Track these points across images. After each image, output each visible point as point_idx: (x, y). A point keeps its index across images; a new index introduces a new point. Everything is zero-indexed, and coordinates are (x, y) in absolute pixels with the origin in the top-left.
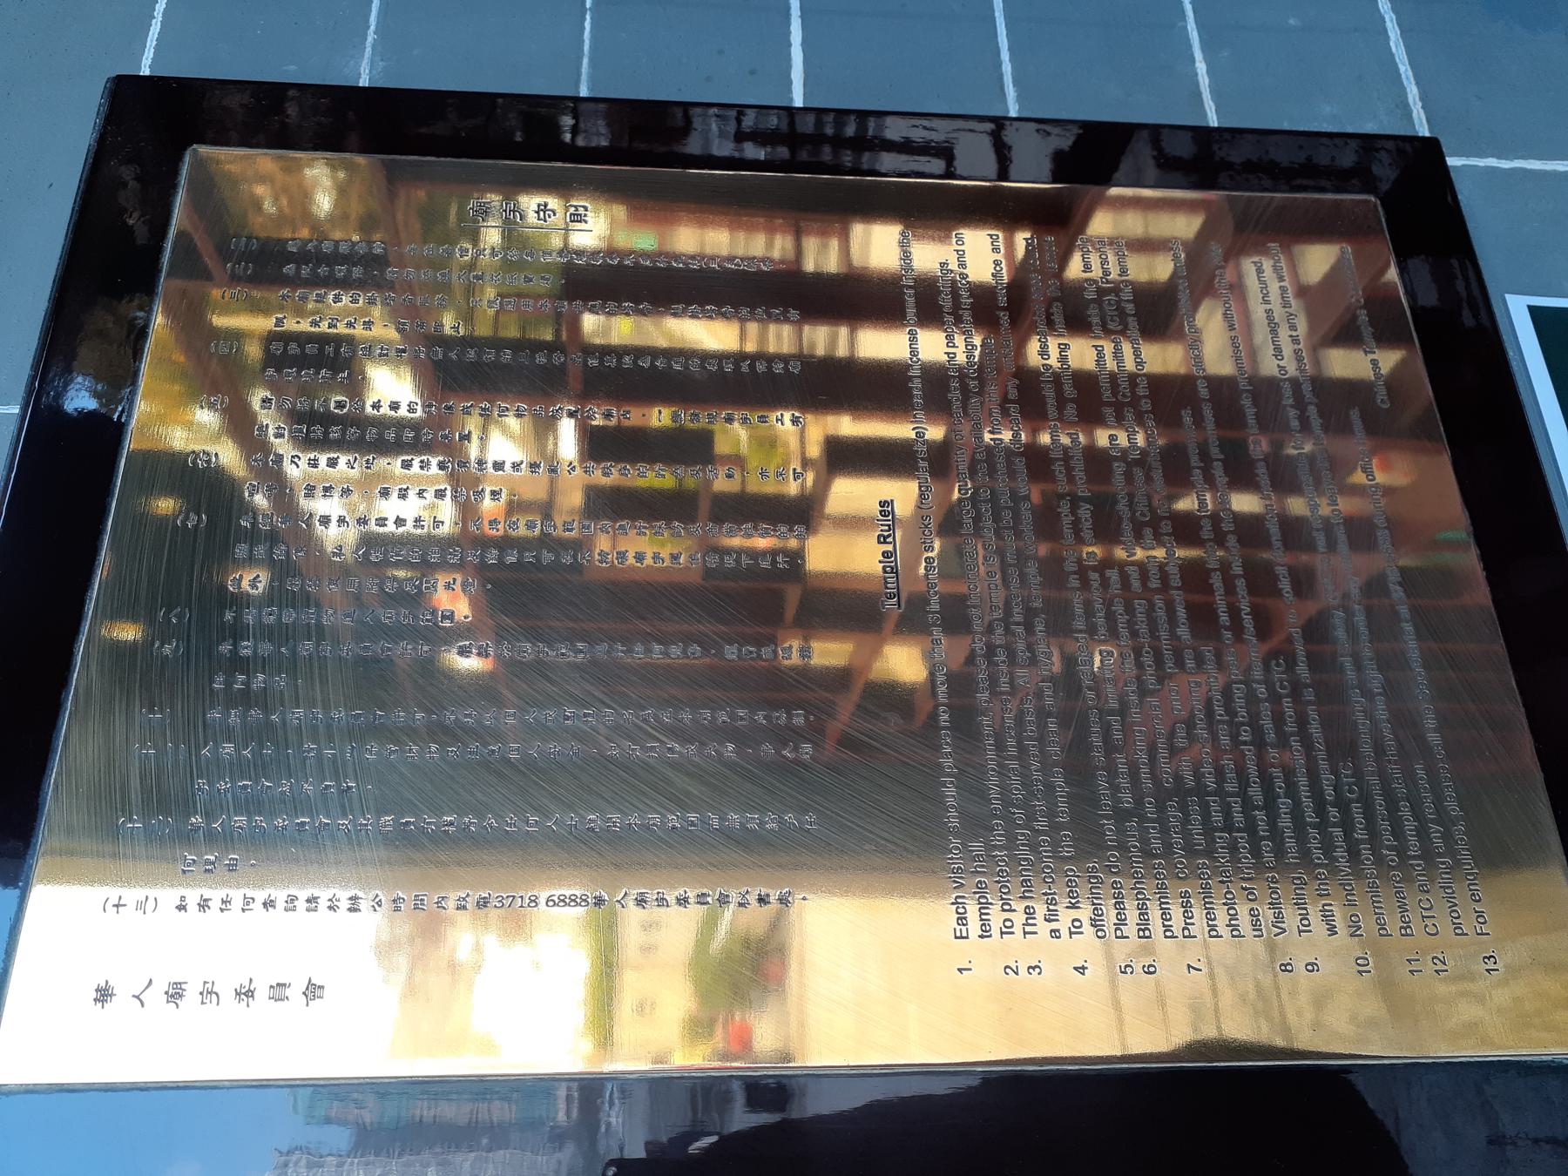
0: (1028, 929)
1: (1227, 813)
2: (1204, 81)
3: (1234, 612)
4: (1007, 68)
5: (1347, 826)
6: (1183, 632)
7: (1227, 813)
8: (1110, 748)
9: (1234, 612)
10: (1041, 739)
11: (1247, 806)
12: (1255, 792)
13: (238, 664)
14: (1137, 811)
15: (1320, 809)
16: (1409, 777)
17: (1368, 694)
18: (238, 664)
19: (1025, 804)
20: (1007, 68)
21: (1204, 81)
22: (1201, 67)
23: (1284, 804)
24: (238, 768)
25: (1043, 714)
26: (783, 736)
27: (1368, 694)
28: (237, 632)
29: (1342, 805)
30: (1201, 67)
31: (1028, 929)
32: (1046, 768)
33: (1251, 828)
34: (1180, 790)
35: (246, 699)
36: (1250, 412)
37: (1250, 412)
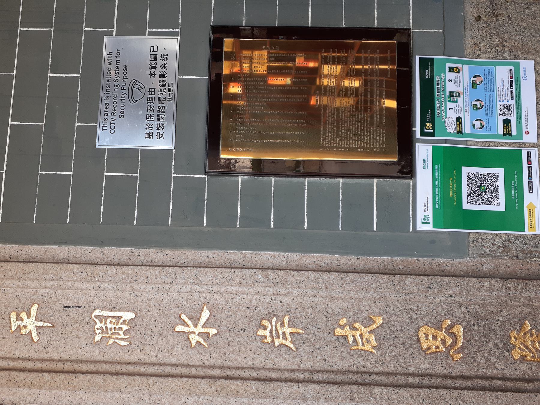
0: (104, 128)
1: (355, 132)
2: (376, 16)
3: (361, 107)
4: (344, 15)
5: (370, 134)
6: (354, 110)
7: (355, 132)
8: (342, 124)
9: (361, 107)
10: (334, 123)
11: (358, 132)
12: (359, 130)
13: (239, 114)
14: (344, 132)
15: (367, 132)
16: (380, 128)
17: (376, 117)
18: (239, 114)
19: (331, 132)
20: (344, 15)
21: (376, 16)
22: (376, 13)
23: (363, 131)
24: (241, 126)
25: (334, 120)
26: (302, 123)
27: (376, 117)
28: (239, 110)
29: (370, 132)
30: (376, 13)
31: (104, 128)
32: (334, 127)
33: (358, 134)
34: (350, 130)
35: (241, 118)
36: (369, 95)
37: (369, 95)
